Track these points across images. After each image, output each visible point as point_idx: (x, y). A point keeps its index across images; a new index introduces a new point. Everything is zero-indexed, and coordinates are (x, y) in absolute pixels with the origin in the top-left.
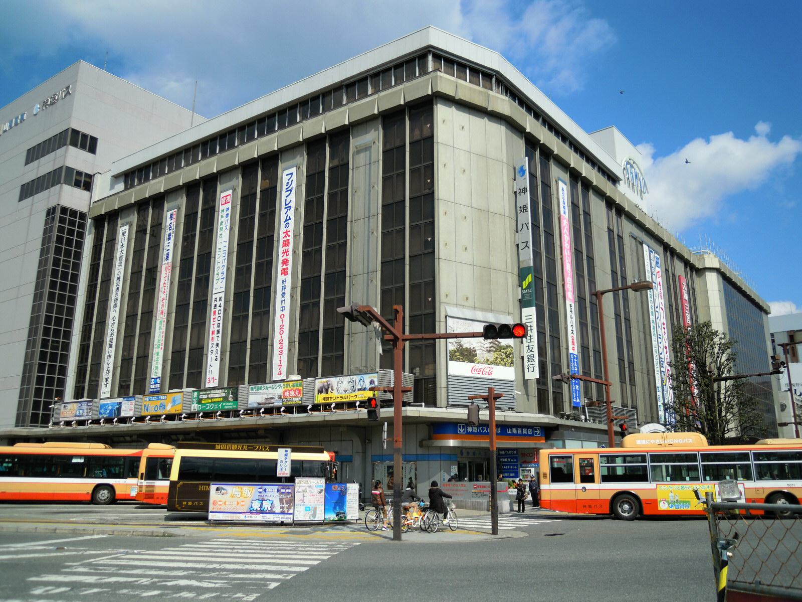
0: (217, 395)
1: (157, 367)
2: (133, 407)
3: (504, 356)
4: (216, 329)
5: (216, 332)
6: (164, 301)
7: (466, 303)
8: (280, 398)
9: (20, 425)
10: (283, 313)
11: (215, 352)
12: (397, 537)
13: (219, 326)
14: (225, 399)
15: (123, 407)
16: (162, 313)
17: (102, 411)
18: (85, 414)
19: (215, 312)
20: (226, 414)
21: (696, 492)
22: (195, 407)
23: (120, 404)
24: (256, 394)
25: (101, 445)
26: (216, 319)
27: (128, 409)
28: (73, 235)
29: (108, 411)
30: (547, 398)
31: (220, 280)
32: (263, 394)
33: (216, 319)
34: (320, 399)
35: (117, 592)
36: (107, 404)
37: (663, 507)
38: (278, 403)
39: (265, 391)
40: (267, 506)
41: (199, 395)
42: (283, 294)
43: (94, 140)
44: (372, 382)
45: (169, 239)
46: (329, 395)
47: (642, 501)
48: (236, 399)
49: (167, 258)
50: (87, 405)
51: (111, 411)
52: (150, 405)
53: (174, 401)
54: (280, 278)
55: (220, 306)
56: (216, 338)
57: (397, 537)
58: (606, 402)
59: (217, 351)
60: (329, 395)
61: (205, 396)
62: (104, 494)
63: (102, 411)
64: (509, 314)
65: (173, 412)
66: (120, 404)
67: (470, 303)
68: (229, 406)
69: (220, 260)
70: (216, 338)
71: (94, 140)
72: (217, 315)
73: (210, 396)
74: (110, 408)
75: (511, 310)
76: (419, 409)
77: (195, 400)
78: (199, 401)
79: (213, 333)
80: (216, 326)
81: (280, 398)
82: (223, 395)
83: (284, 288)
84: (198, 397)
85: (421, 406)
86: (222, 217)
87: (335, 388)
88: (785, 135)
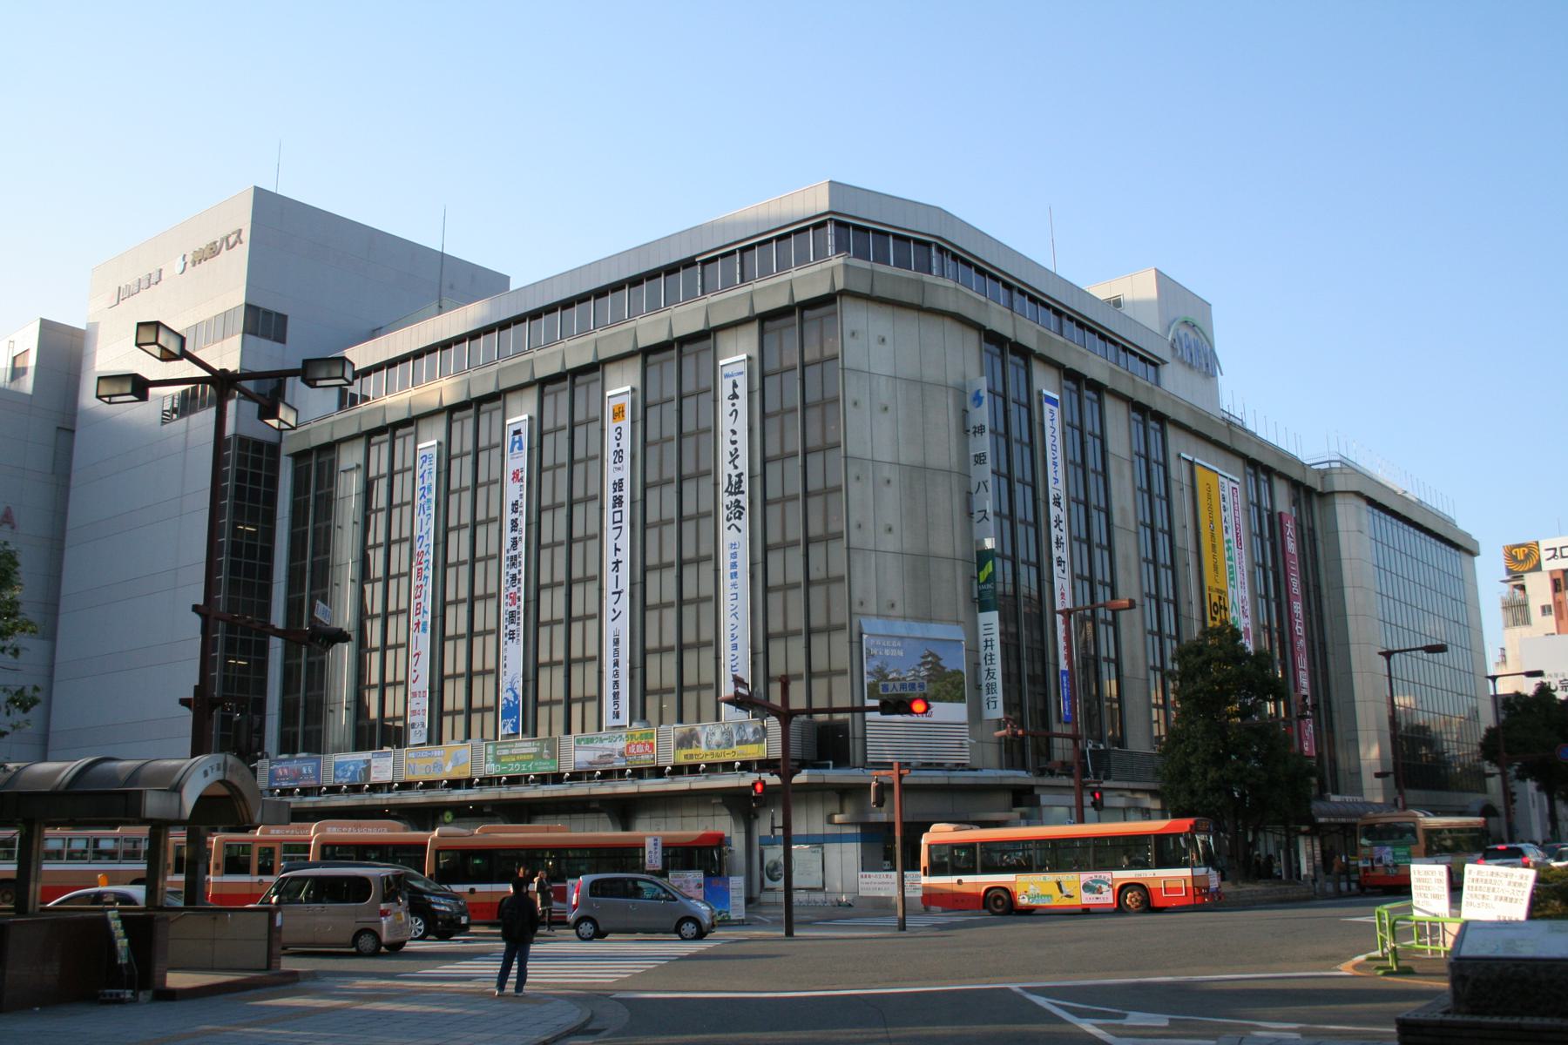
3: (949, 687)
7: (891, 612)
8: (622, 754)
12: (789, 933)
14: (538, 756)
17: (340, 773)
20: (543, 779)
21: (1059, 884)
23: (368, 762)
25: (950, 827)
28: (257, 502)
32: (595, 749)
34: (681, 757)
37: (1023, 901)
38: (619, 764)
39: (599, 745)
41: (495, 750)
43: (282, 319)
51: (354, 773)
53: (456, 759)
57: (789, 933)
61: (506, 752)
62: (1131, 898)
63: (340, 773)
64: (958, 622)
65: (456, 775)
66: (368, 762)
67: (899, 610)
71: (282, 319)
75: (961, 618)
76: (824, 771)
77: (490, 758)
78: (497, 760)
81: (622, 754)
82: (534, 750)
85: (827, 767)
87: (703, 739)
88: (1102, 302)
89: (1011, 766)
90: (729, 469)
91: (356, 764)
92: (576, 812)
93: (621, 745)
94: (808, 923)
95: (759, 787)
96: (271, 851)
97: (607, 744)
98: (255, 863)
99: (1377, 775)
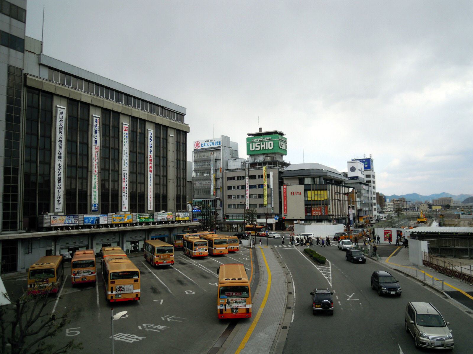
0: (146, 216)
1: (95, 199)
2: (106, 219)
4: (125, 186)
5: (125, 188)
6: (96, 166)
9: (10, 230)
10: (151, 186)
11: (125, 196)
13: (126, 186)
14: (149, 218)
15: (100, 219)
16: (96, 171)
17: (86, 221)
18: (73, 222)
19: (124, 179)
22: (138, 220)
23: (98, 217)
24: (159, 216)
26: (125, 182)
27: (103, 220)
29: (91, 221)
30: (120, 195)
31: (126, 166)
33: (125, 182)
34: (177, 219)
35: (200, 224)
36: (90, 217)
40: (70, 221)
41: (139, 216)
42: (151, 179)
44: (188, 215)
45: (96, 133)
46: (179, 218)
47: (188, 163)
48: (153, 217)
49: (96, 143)
50: (74, 217)
51: (93, 221)
52: (117, 218)
53: (128, 218)
54: (149, 173)
55: (126, 177)
56: (125, 191)
58: (347, 215)
59: (126, 196)
60: (179, 218)
61: (142, 216)
63: (86, 221)
66: (98, 217)
68: (151, 220)
69: (125, 156)
70: (125, 191)
72: (125, 181)
73: (144, 216)
74: (92, 219)
78: (140, 218)
79: (124, 188)
80: (125, 185)
81: (167, 218)
82: (149, 216)
83: (151, 177)
84: (139, 216)
86: (125, 136)
89: (196, 152)
90: (127, 184)
91: (93, 218)
92: (180, 250)
93: (166, 216)
94: (316, 295)
95: (191, 244)
96: (238, 198)
97: (164, 216)
98: (240, 187)
99: (375, 276)
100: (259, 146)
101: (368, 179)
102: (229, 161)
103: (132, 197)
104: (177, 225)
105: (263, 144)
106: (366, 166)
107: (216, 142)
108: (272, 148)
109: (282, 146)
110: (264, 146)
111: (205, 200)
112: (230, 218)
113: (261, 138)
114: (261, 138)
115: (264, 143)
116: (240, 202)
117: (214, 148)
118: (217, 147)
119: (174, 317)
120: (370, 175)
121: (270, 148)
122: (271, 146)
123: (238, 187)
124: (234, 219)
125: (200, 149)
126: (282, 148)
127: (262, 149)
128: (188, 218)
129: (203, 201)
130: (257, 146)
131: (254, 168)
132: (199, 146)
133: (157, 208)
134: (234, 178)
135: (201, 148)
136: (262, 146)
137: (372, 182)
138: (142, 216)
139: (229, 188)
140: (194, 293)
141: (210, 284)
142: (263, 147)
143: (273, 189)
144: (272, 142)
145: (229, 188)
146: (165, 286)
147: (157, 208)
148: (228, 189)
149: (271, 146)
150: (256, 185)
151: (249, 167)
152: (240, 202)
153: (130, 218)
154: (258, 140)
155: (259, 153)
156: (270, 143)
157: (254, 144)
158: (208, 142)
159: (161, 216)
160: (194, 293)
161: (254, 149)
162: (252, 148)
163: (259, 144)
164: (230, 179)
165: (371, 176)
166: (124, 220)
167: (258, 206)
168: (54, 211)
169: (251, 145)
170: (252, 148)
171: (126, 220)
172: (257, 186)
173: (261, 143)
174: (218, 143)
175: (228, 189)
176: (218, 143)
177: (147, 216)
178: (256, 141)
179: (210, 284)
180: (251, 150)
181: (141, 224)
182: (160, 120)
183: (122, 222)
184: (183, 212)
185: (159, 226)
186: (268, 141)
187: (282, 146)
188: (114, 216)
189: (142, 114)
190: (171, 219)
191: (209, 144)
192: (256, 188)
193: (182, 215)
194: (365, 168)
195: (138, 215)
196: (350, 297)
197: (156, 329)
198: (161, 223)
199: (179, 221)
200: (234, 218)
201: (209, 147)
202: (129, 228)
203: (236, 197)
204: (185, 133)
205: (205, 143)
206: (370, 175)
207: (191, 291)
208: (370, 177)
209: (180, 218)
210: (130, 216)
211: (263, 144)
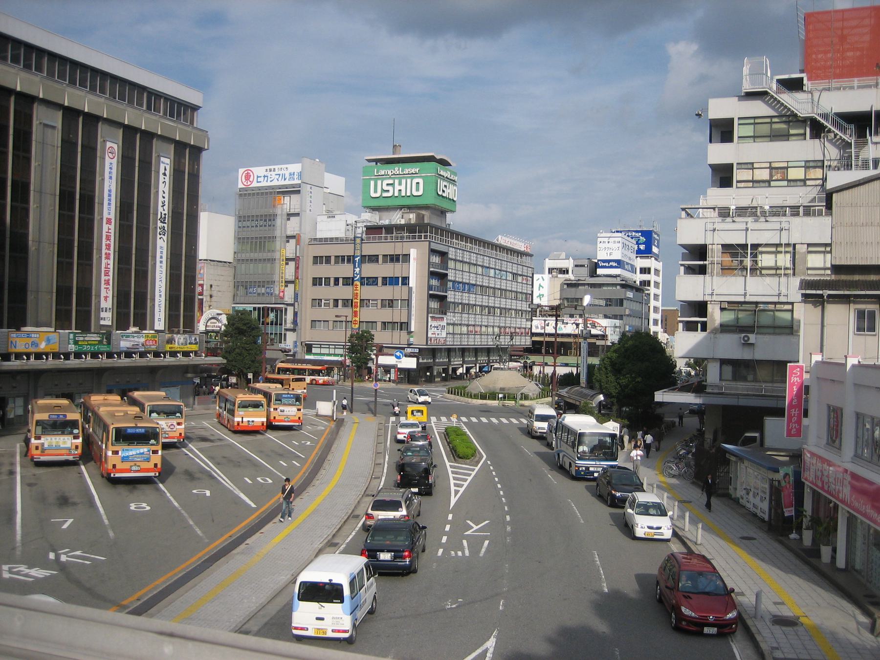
14: (100, 342)
22: (72, 348)
34: (168, 347)
41: (75, 337)
48: (109, 343)
61: (81, 339)
78: (76, 343)
93: (142, 340)
97: (136, 339)
100: (390, 188)
101: (645, 277)
102: (319, 219)
103: (63, 294)
104: (169, 360)
105: (400, 184)
106: (642, 247)
107: (290, 174)
108: (420, 193)
109: (444, 191)
110: (403, 188)
111: (259, 308)
112: (314, 350)
113: (396, 169)
114: (396, 169)
115: (404, 181)
116: (337, 316)
117: (286, 186)
118: (293, 186)
119: (78, 553)
120: (649, 269)
121: (415, 193)
122: (418, 190)
123: (337, 280)
124: (324, 354)
125: (253, 189)
126: (444, 195)
127: (396, 194)
128: (195, 347)
129: (255, 309)
130: (385, 188)
131: (374, 238)
132: (251, 179)
133: (122, 322)
134: (328, 259)
135: (255, 185)
136: (397, 187)
137: (652, 284)
138: (81, 339)
139: (317, 281)
140: (148, 508)
141: (194, 491)
142: (400, 190)
143: (414, 290)
144: (421, 181)
145: (317, 281)
146: (176, 504)
147: (122, 322)
148: (314, 284)
149: (418, 190)
150: (377, 278)
151: (364, 236)
152: (337, 316)
153: (52, 342)
154: (390, 173)
155: (389, 203)
156: (415, 181)
157: (379, 182)
158: (272, 173)
159: (130, 339)
160: (148, 508)
161: (378, 195)
162: (376, 191)
163: (391, 182)
164: (317, 260)
165: (652, 271)
166: (37, 345)
167: (379, 325)
168: (152, 328)
169: (372, 183)
170: (376, 191)
171: (43, 346)
172: (380, 281)
173: (397, 182)
174: (296, 177)
175: (314, 284)
176: (296, 177)
177: (93, 338)
178: (383, 177)
179: (194, 491)
180: (373, 195)
181: (78, 355)
182: (131, 116)
183: (32, 349)
184: (185, 332)
185: (124, 362)
186: (412, 175)
187: (444, 191)
188: (14, 335)
189: (87, 101)
190: (154, 348)
191: (274, 176)
192: (377, 284)
193: (182, 341)
194: (639, 252)
195: (72, 336)
196: (476, 528)
197: (27, 575)
198: (129, 355)
199: (173, 354)
200: (324, 351)
201: (275, 183)
202: (50, 363)
203: (332, 302)
204: (197, 151)
205: (266, 174)
206: (649, 269)
207: (144, 505)
208: (649, 273)
209: (176, 346)
210: (54, 337)
211: (400, 184)
